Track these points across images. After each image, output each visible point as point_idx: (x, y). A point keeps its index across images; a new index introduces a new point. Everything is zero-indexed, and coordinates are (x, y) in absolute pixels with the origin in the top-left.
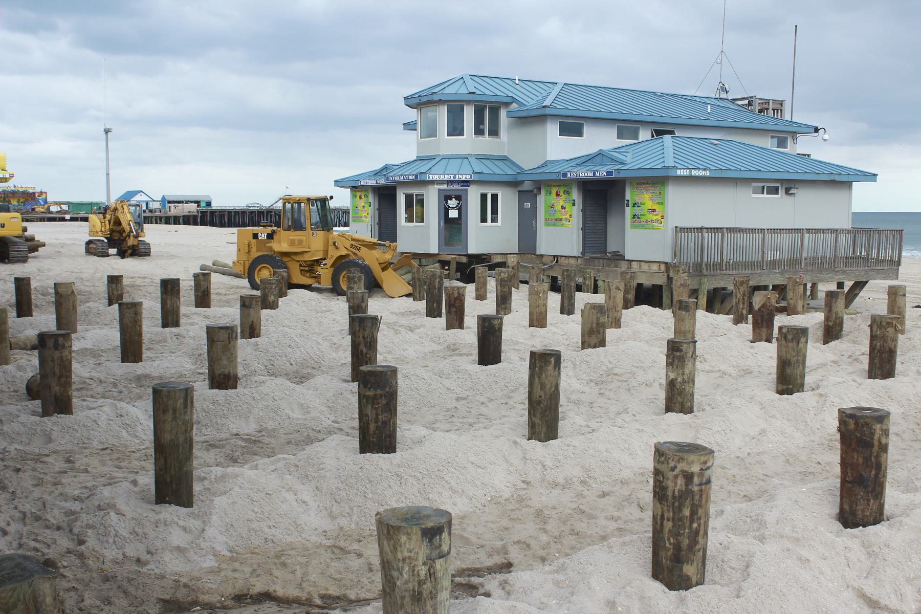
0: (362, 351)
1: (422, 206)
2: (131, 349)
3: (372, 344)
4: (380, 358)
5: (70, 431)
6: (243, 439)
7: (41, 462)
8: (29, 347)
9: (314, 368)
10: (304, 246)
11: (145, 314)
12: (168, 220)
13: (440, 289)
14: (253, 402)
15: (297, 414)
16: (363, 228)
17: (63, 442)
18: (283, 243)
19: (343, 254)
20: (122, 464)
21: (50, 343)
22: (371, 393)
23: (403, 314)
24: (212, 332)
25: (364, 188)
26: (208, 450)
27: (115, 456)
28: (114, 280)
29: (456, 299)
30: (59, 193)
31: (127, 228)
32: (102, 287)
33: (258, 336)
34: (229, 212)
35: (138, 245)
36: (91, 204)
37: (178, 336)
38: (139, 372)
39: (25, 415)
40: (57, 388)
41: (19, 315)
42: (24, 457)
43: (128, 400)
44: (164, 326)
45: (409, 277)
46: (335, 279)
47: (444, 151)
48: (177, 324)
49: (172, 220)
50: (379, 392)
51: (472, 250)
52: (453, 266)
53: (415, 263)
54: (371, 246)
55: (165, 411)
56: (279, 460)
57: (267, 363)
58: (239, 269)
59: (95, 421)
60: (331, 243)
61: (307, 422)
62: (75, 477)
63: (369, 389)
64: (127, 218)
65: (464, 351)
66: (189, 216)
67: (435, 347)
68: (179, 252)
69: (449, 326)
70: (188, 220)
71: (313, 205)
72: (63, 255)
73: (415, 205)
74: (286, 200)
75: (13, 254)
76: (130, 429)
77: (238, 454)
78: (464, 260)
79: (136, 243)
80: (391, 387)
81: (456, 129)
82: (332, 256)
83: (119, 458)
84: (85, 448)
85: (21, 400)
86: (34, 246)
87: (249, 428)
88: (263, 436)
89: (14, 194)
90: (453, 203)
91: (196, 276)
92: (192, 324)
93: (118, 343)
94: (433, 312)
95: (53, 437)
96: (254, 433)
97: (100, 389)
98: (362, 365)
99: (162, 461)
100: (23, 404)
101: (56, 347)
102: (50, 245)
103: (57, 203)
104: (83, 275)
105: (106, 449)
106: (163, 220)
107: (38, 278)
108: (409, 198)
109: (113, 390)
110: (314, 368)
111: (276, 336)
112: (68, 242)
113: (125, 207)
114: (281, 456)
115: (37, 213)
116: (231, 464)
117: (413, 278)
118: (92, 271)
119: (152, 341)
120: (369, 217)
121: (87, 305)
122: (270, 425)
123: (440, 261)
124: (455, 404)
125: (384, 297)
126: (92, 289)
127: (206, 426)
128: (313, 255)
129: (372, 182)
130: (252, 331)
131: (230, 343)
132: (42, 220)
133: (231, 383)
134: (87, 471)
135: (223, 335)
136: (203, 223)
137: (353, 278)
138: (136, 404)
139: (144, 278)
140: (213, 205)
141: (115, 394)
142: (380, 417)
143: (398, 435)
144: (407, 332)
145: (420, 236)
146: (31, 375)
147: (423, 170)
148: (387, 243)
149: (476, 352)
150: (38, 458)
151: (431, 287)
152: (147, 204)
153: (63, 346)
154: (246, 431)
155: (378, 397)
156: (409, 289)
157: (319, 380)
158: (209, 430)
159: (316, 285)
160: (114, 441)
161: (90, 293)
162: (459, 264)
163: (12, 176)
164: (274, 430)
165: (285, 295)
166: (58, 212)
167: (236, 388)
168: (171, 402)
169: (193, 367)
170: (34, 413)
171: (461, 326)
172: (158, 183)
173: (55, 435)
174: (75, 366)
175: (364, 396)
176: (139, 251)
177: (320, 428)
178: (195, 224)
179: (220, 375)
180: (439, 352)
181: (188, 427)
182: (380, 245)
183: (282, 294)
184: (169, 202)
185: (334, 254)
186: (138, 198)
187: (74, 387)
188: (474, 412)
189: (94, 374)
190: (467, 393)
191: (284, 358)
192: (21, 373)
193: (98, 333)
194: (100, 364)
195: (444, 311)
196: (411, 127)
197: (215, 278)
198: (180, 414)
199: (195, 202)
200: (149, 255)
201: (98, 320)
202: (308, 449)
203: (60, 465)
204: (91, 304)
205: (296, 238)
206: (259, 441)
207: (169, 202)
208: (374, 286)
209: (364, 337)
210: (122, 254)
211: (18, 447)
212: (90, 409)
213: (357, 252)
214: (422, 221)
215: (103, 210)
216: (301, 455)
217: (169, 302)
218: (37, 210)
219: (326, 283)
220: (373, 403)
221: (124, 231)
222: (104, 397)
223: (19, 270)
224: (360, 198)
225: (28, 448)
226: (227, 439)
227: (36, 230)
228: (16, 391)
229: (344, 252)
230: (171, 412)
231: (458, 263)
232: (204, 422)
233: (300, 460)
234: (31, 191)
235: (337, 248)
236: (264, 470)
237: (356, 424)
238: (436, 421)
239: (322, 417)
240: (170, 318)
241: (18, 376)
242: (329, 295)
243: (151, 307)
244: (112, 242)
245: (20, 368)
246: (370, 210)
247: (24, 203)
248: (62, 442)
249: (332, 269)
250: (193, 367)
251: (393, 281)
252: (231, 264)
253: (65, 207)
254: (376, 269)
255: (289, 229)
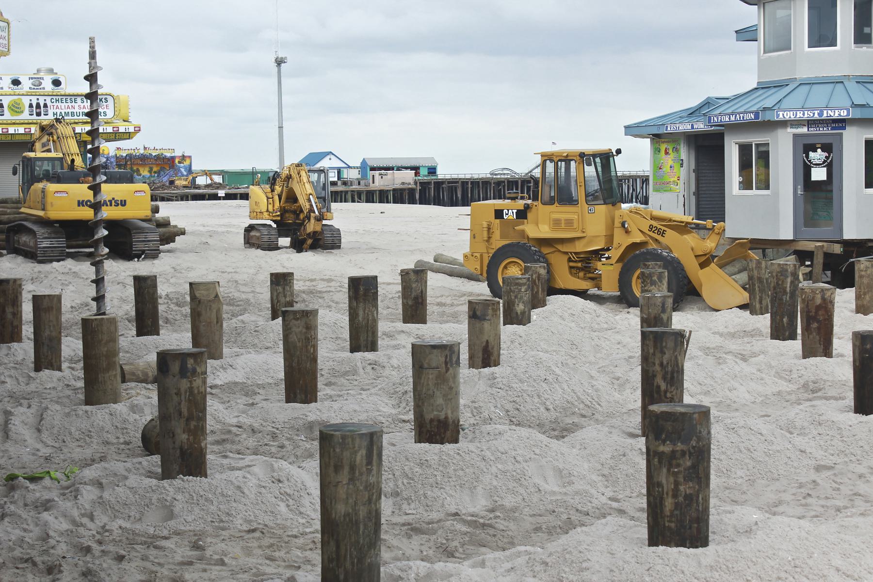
0: (659, 387)
1: (767, 165)
2: (300, 383)
3: (675, 376)
4: (687, 400)
5: (202, 501)
6: (465, 522)
7: (156, 547)
8: (151, 379)
9: (584, 416)
10: (575, 230)
11: (322, 333)
12: (370, 197)
13: (793, 294)
14: (482, 465)
15: (552, 485)
16: (672, 202)
17: (190, 519)
18: (541, 225)
19: (638, 240)
20: (277, 554)
21: (175, 367)
22: (666, 448)
23: (733, 335)
24: (419, 352)
25: (673, 138)
26: (409, 537)
27: (267, 541)
28: (281, 280)
29: (818, 308)
30: (208, 159)
31: (306, 206)
32: (264, 294)
33: (496, 364)
34: (464, 183)
35: (322, 232)
36: (253, 173)
37: (374, 364)
38: (312, 417)
39: (139, 475)
40: (184, 437)
41: (139, 334)
42: (131, 539)
43: (292, 459)
44: (353, 350)
45: (743, 277)
46: (624, 282)
47: (803, 73)
48: (372, 347)
49: (376, 197)
50: (680, 446)
51: (850, 233)
52: (819, 259)
53: (754, 255)
54: (683, 228)
55: (338, 468)
56: (519, 555)
57: (509, 406)
58: (474, 267)
59: (239, 488)
60: (617, 224)
61: (568, 498)
62: (205, 570)
63: (664, 442)
64: (305, 191)
65: (832, 393)
66: (402, 190)
67: (784, 386)
68: (380, 240)
69: (808, 353)
70: (401, 196)
71: (589, 165)
72: (211, 246)
73: (756, 162)
74: (547, 158)
75: (138, 247)
76: (291, 502)
77: (456, 543)
78: (838, 249)
79: (318, 229)
80: (699, 439)
81: (822, 34)
82: (620, 245)
83: (272, 545)
84: (223, 529)
85: (134, 456)
86: (168, 234)
87: (476, 505)
88: (497, 517)
89: (144, 159)
90: (817, 156)
91: (405, 274)
92: (396, 347)
93: (282, 375)
94: (781, 332)
95: (177, 510)
96: (484, 513)
97: (251, 442)
98: (652, 404)
99: (333, 546)
100: (135, 460)
101: (183, 372)
102: (193, 233)
103: (206, 173)
104: (237, 277)
105: (254, 531)
106: (363, 197)
107: (172, 281)
108: (745, 150)
109: (271, 442)
110: (584, 416)
111: (524, 363)
112: (220, 230)
113: (303, 174)
114: (522, 548)
115: (177, 187)
116: (444, 558)
117: (751, 278)
118: (252, 271)
119: (334, 372)
120: (681, 183)
121: (240, 318)
122: (509, 501)
123: (797, 253)
124: (813, 475)
125: (704, 310)
126: (250, 296)
127: (408, 500)
128: (590, 243)
129: (685, 127)
130: (486, 356)
131: (447, 370)
132: (184, 198)
133: (449, 433)
134: (222, 563)
135: (437, 359)
136: (424, 201)
137: (650, 275)
138: (303, 465)
139: (330, 280)
140: (438, 172)
141: (273, 450)
142: (682, 488)
143: (713, 519)
144: (731, 355)
145: (763, 211)
146: (149, 418)
147: (768, 103)
148: (709, 223)
149: (851, 395)
150: (152, 542)
151: (778, 291)
152: (339, 173)
153: (194, 372)
154: (471, 510)
155: (678, 455)
156: (744, 297)
157: (589, 433)
158: (413, 506)
159: (593, 291)
160: (268, 519)
161: (247, 301)
162: (828, 257)
163: (138, 130)
164: (514, 510)
165: (543, 304)
166: (207, 186)
167: (456, 441)
168: (346, 454)
169: (394, 411)
170: (150, 474)
171: (827, 351)
172: (355, 141)
173: (178, 508)
174: (213, 406)
175: (656, 453)
176: (324, 241)
177: (588, 507)
178: (412, 201)
179: (432, 421)
180: (789, 393)
181: (374, 493)
182: (698, 227)
183: (537, 303)
184: (373, 169)
185: (622, 241)
186: (324, 163)
187: (210, 439)
188: (845, 490)
189: (245, 420)
190: (835, 459)
191: (536, 400)
192: (137, 417)
193: (253, 359)
194: (253, 404)
195: (799, 331)
196: (749, 36)
197: (435, 282)
198: (361, 474)
199: (412, 168)
200: (339, 247)
201: (256, 341)
202: (564, 540)
203: (182, 551)
204: (245, 317)
205: (563, 216)
206: (490, 526)
207: (373, 169)
208: (686, 292)
209: (661, 364)
210: (298, 246)
211: (127, 525)
212: (232, 469)
213: (659, 237)
214: (767, 187)
215: (272, 179)
216: (552, 547)
217: (361, 313)
218: (177, 183)
219: (610, 288)
220: (670, 466)
221: (302, 211)
222: (255, 453)
223: (142, 267)
224: (667, 153)
225: (138, 527)
226: (439, 521)
227: (173, 212)
228: (127, 443)
229: (638, 238)
230: (346, 470)
231: (827, 255)
232: (405, 494)
233: (550, 554)
234: (168, 155)
235: (627, 232)
236: (494, 569)
237: (643, 503)
238: (780, 503)
239: (593, 491)
240: (363, 337)
241: (131, 420)
242: (614, 306)
243: (333, 321)
244: (283, 228)
245: (134, 408)
246: (683, 172)
247: (158, 172)
248: (189, 519)
249: (620, 265)
250: (394, 411)
251: (714, 282)
252: (461, 259)
253: (218, 179)
254: (691, 265)
255: (551, 201)
